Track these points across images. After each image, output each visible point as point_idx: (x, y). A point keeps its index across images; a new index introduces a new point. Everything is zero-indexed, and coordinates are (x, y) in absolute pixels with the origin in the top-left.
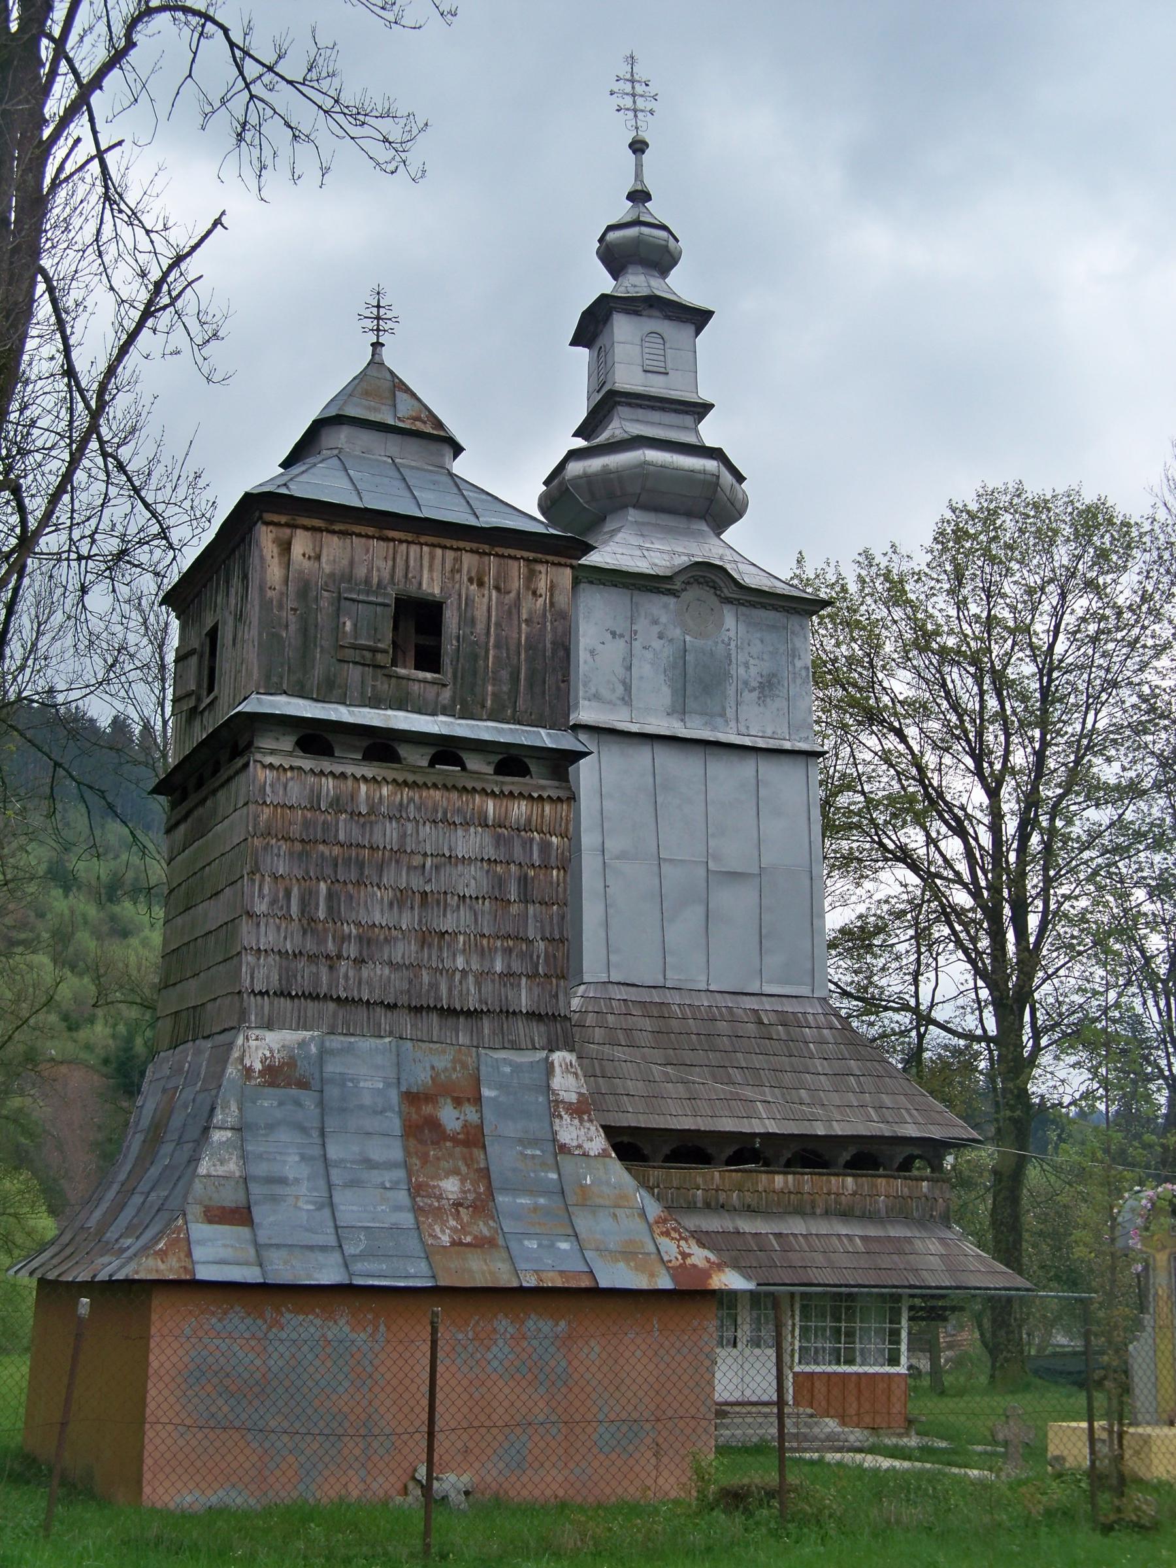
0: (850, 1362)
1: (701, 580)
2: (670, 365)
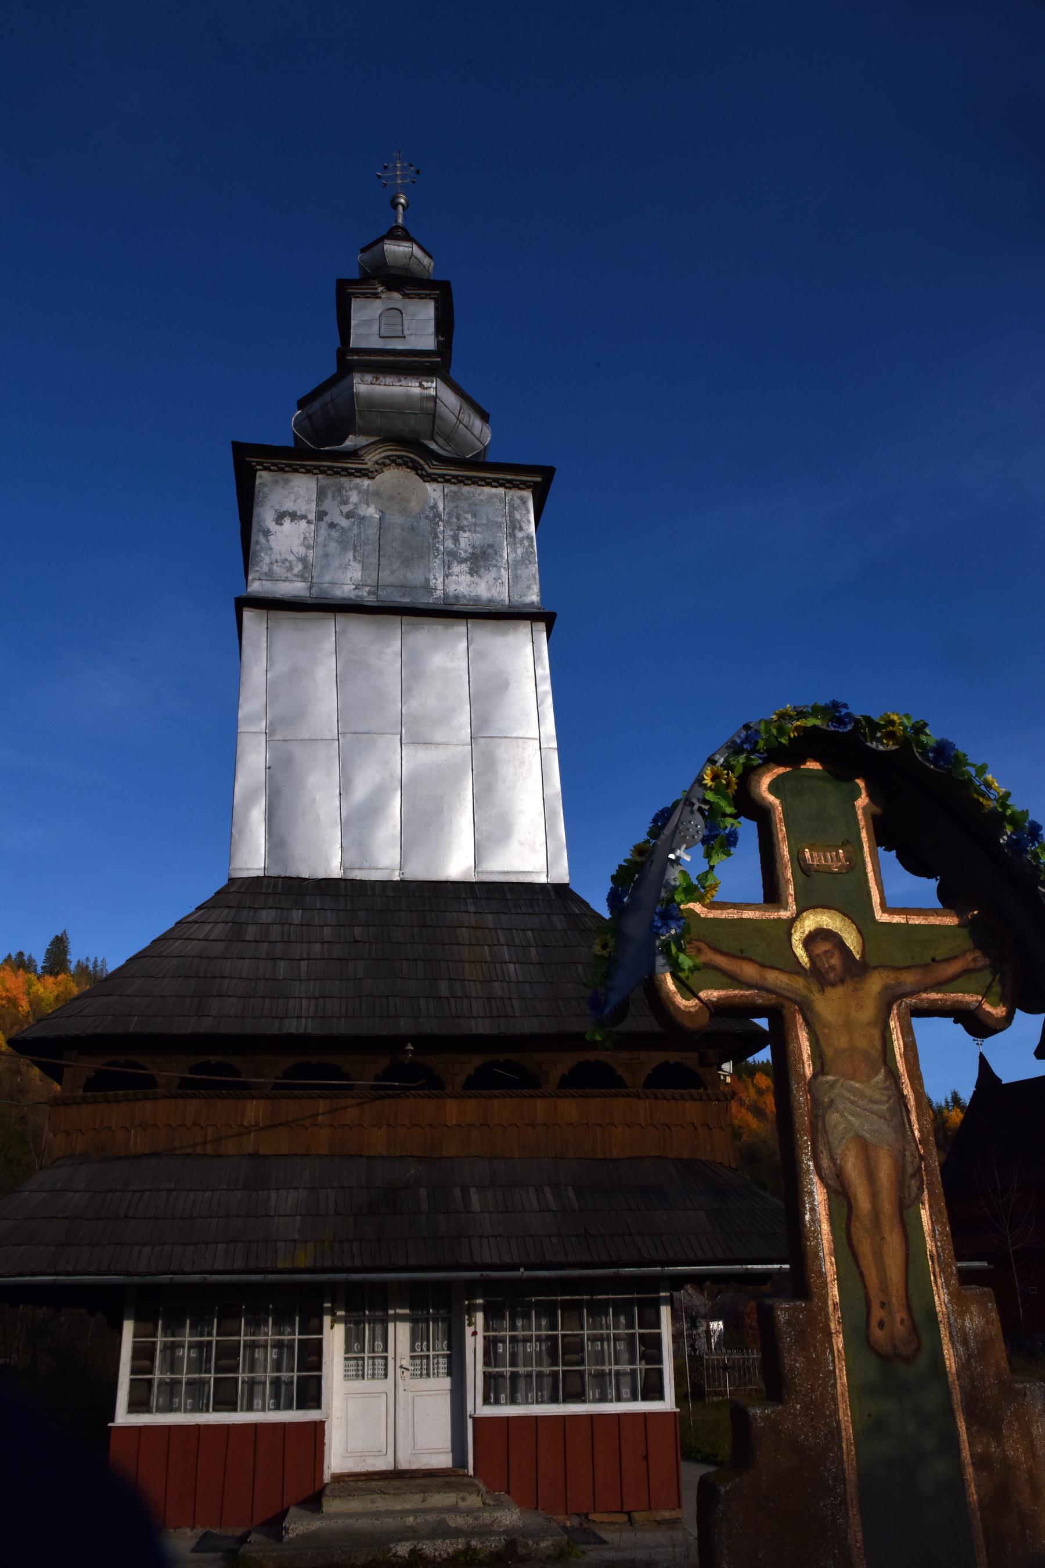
0: (579, 1396)
1: (399, 461)
2: (406, 333)
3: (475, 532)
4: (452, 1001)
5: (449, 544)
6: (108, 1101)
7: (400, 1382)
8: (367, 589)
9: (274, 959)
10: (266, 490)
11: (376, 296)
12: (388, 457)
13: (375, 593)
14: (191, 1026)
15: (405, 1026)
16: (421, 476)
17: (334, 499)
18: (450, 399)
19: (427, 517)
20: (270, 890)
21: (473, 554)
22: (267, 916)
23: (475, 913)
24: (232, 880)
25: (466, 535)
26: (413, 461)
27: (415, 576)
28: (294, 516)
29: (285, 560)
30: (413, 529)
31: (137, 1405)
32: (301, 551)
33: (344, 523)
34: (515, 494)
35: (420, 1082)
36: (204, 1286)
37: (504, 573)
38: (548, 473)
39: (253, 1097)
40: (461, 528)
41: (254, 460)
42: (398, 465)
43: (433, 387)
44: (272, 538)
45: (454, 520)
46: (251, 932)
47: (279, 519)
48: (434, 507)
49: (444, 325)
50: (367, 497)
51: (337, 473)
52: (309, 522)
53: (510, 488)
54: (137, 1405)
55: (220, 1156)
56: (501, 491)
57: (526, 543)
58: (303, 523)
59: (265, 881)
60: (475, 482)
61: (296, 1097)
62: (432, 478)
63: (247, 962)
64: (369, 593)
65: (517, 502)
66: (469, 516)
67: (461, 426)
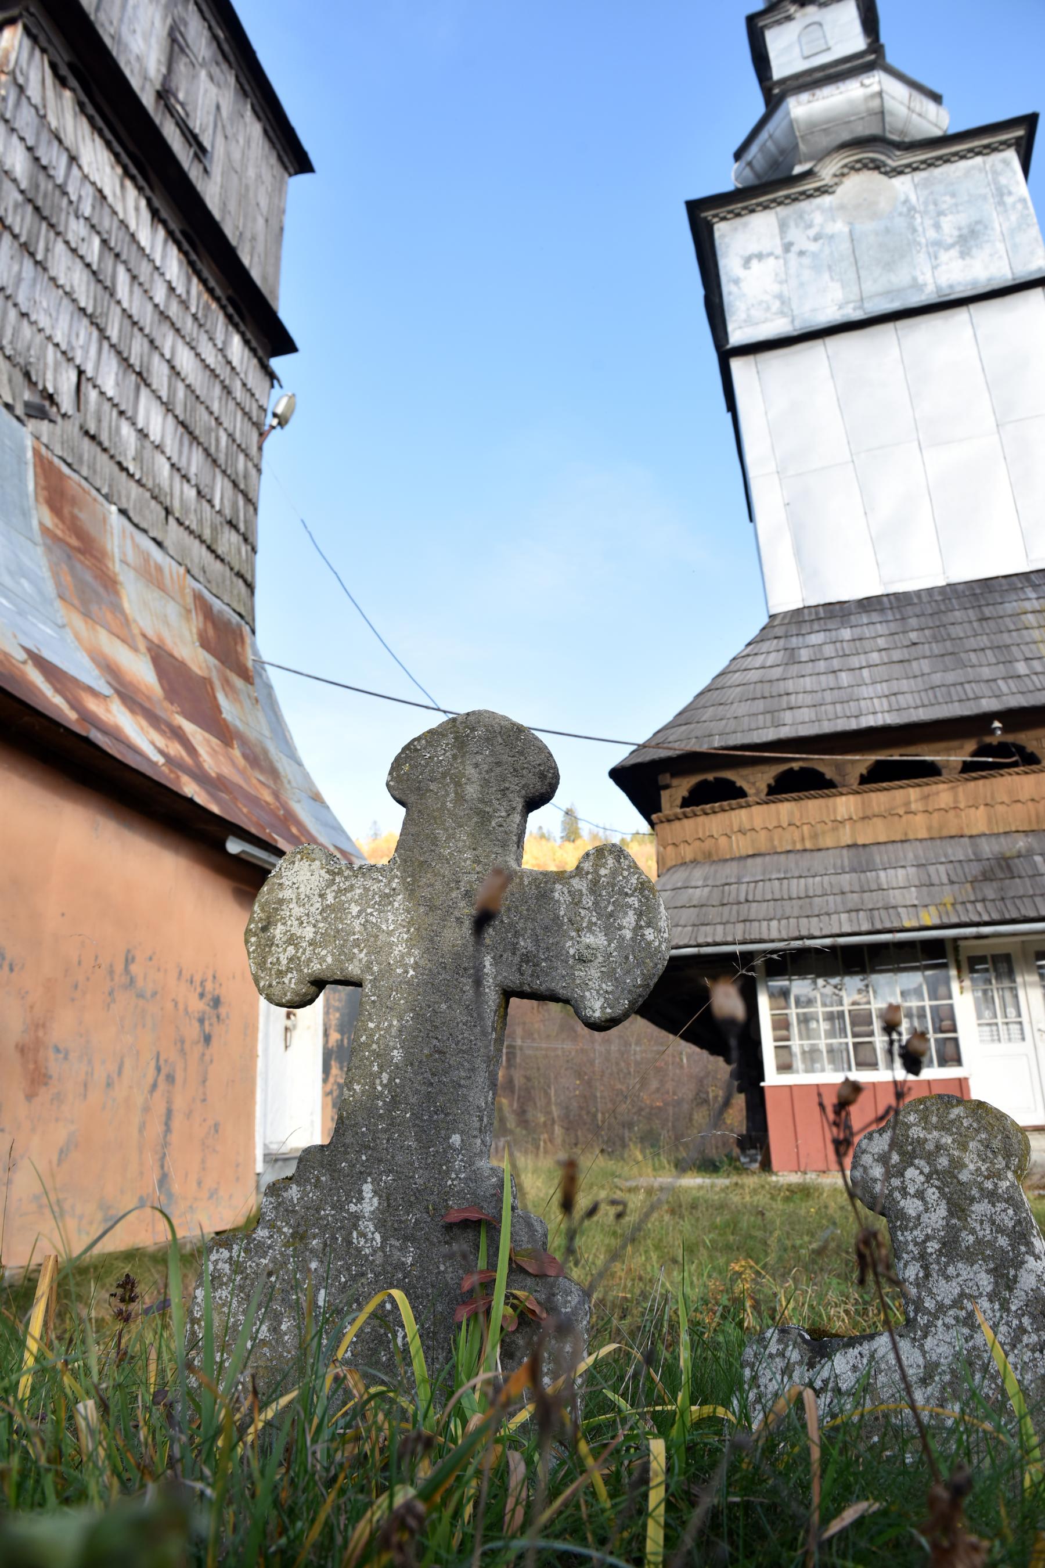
1: (858, 166)
2: (831, 43)
3: (958, 212)
4: (1034, 677)
5: (932, 234)
6: (706, 814)
7: (1039, 1044)
8: (852, 305)
9: (834, 672)
10: (727, 240)
11: (789, 18)
12: (845, 166)
13: (861, 307)
14: (770, 735)
15: (989, 705)
16: (886, 173)
17: (797, 226)
18: (896, 92)
19: (900, 214)
20: (813, 617)
21: (960, 236)
22: (816, 639)
23: (1038, 598)
24: (772, 617)
25: (949, 218)
26: (873, 160)
27: (901, 277)
28: (760, 256)
29: (761, 302)
30: (887, 231)
31: (785, 1067)
32: (776, 288)
33: (813, 247)
34: (996, 158)
35: (1014, 759)
36: (833, 948)
37: (1000, 246)
38: (1030, 121)
39: (842, 794)
40: (941, 213)
41: (708, 214)
42: (858, 170)
43: (876, 80)
44: (742, 285)
45: (931, 207)
46: (804, 654)
47: (747, 262)
48: (906, 201)
49: (870, 23)
50: (831, 213)
51: (795, 200)
52: (777, 258)
53: (988, 154)
54: (785, 1067)
55: (819, 850)
56: (979, 160)
57: (1019, 206)
58: (771, 260)
59: (806, 611)
60: (946, 160)
61: (886, 789)
62: (899, 172)
63: (808, 679)
64: (855, 309)
65: (1000, 167)
66: (947, 198)
67: (914, 116)
